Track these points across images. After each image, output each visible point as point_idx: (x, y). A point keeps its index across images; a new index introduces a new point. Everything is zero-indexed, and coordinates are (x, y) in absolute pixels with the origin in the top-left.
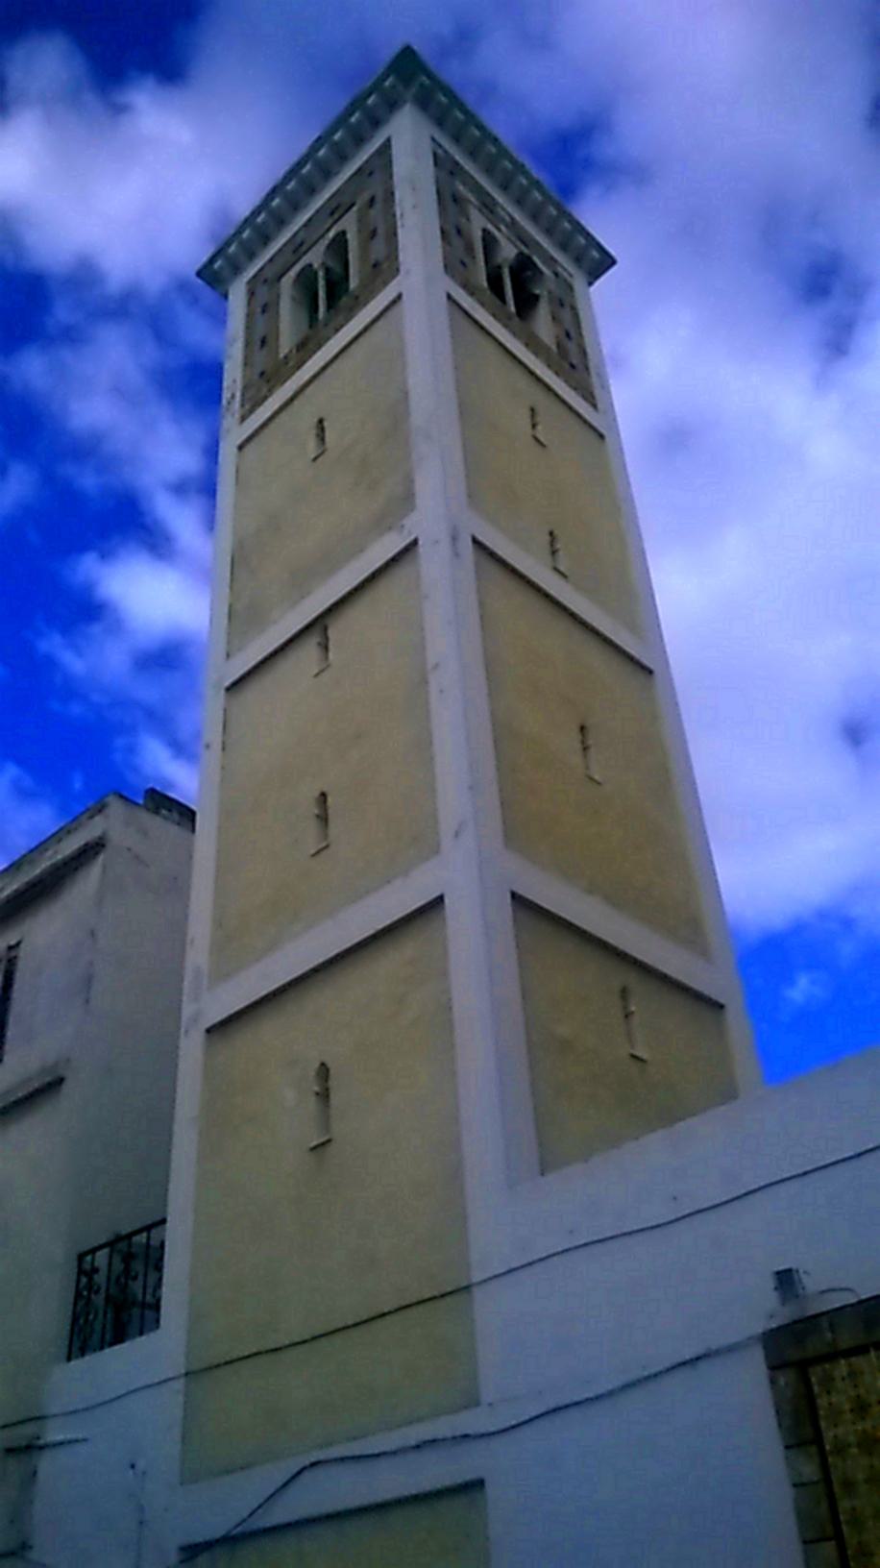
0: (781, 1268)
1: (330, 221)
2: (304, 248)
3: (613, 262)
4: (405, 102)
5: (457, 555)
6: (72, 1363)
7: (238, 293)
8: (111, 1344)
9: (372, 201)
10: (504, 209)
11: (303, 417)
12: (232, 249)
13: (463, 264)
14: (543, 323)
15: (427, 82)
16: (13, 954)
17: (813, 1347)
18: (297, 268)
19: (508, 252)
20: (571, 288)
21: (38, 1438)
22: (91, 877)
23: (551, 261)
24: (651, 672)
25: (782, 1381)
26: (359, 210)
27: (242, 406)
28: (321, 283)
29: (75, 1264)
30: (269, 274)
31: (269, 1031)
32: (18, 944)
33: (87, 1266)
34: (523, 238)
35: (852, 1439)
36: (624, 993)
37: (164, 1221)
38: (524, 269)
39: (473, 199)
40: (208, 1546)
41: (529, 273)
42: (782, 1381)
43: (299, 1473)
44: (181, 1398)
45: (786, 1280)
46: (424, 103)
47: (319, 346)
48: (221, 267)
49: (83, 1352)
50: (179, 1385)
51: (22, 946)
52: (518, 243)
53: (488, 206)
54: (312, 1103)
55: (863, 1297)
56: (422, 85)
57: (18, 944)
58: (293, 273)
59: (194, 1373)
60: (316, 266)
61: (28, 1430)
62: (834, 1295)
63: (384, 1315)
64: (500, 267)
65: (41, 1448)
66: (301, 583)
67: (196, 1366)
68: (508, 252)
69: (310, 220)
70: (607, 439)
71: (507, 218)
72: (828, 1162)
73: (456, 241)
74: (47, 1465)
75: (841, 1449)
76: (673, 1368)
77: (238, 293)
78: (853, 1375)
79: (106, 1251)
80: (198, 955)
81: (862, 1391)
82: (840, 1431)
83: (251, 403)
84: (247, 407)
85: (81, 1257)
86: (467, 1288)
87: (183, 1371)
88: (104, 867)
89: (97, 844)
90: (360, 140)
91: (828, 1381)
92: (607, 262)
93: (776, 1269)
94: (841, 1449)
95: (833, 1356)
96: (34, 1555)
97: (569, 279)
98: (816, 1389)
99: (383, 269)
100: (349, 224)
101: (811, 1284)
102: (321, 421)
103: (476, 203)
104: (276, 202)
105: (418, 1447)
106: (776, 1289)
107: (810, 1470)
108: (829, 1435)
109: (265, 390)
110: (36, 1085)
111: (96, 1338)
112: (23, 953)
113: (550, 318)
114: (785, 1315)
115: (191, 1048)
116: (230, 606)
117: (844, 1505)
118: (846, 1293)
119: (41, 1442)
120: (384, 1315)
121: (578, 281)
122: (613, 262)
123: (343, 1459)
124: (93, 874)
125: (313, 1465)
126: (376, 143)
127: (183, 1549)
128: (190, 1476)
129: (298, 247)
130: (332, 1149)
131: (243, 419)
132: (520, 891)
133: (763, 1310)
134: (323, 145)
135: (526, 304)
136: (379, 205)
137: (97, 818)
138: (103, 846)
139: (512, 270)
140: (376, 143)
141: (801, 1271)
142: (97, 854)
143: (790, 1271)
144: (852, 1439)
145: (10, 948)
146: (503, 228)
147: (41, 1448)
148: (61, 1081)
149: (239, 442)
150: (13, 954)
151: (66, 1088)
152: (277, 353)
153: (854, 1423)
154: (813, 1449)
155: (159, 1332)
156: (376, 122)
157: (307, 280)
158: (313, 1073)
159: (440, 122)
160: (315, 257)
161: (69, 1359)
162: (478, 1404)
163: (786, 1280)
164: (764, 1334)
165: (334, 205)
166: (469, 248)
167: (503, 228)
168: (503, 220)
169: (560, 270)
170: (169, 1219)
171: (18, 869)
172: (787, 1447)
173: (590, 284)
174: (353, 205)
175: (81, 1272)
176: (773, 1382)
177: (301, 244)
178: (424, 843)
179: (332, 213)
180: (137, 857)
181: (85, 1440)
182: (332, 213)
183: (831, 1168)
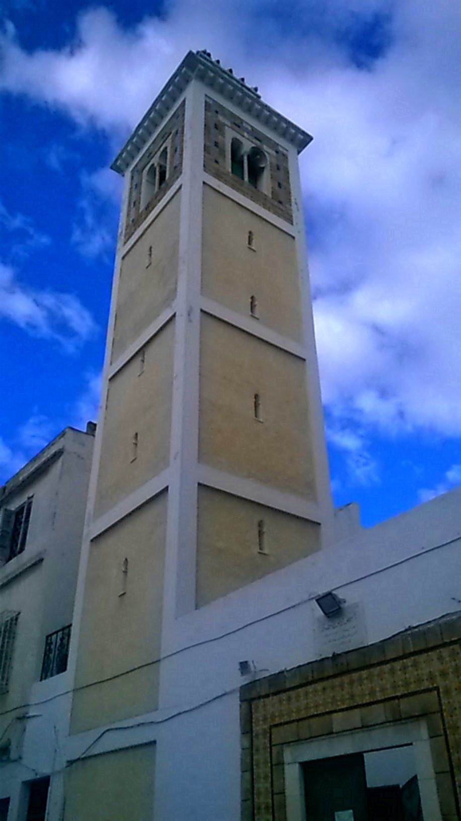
1: (162, 142)
2: (152, 155)
3: (311, 139)
4: (191, 80)
5: (190, 321)
6: (43, 681)
7: (128, 174)
8: (58, 673)
9: (177, 133)
10: (247, 123)
11: (143, 247)
12: (124, 155)
13: (216, 162)
14: (266, 183)
15: (202, 67)
16: (30, 500)
17: (254, 694)
18: (149, 166)
19: (247, 146)
20: (285, 157)
21: (27, 713)
22: (56, 469)
23: (275, 146)
24: (304, 360)
25: (243, 707)
26: (172, 136)
27: (125, 237)
28: (157, 173)
29: (45, 640)
30: (139, 167)
31: (111, 542)
32: (32, 496)
33: (49, 641)
34: (257, 136)
36: (260, 524)
37: (71, 625)
38: (256, 155)
39: (226, 123)
40: (75, 761)
41: (258, 157)
42: (243, 707)
43: (104, 733)
44: (71, 700)
46: (202, 77)
47: (153, 208)
48: (120, 164)
49: (45, 678)
50: (70, 695)
51: (34, 497)
52: (254, 141)
53: (238, 124)
54: (122, 575)
56: (199, 69)
57: (32, 496)
58: (147, 169)
59: (77, 689)
60: (156, 165)
61: (24, 710)
62: (263, 672)
63: (135, 669)
64: (243, 156)
65: (29, 717)
66: (137, 333)
67: (78, 687)
68: (247, 146)
69: (155, 140)
70: (296, 239)
71: (250, 128)
73: (214, 150)
74: (31, 725)
76: (215, 699)
77: (128, 174)
79: (61, 632)
80: (90, 507)
82: (258, 728)
83: (129, 236)
84: (127, 237)
85: (47, 637)
86: (159, 661)
87: (73, 688)
88: (63, 465)
89: (59, 452)
90: (174, 100)
92: (308, 139)
95: (259, 698)
96: (24, 761)
97: (285, 152)
99: (177, 170)
100: (168, 143)
102: (151, 248)
103: (229, 125)
104: (140, 132)
105: (138, 725)
106: (239, 669)
107: (247, 744)
109: (133, 229)
110: (33, 562)
111: (54, 672)
112: (34, 500)
113: (270, 176)
114: (245, 680)
115: (86, 546)
116: (114, 339)
118: (266, 672)
119: (27, 715)
120: (135, 669)
121: (291, 150)
122: (311, 139)
123: (117, 729)
124: (59, 465)
125: (108, 730)
126: (179, 102)
127: (68, 762)
128: (73, 730)
129: (150, 155)
130: (125, 596)
131: (125, 243)
132: (201, 482)
134: (157, 103)
135: (255, 174)
136: (179, 135)
137: (62, 439)
138: (62, 453)
139: (248, 156)
140: (179, 102)
142: (60, 456)
143: (246, 662)
145: (29, 498)
146: (246, 134)
147: (29, 717)
148: (41, 560)
149: (122, 256)
150: (30, 500)
151: (44, 563)
152: (139, 210)
154: (249, 735)
155: (66, 672)
156: (181, 90)
157: (152, 169)
158: (122, 563)
159: (211, 84)
160: (155, 160)
161: (41, 680)
162: (157, 710)
163: (244, 666)
164: (241, 687)
165: (163, 133)
166: (222, 153)
167: (246, 134)
168: (246, 130)
169: (281, 149)
170: (73, 625)
171: (35, 460)
172: (243, 733)
173: (299, 153)
174: (170, 133)
175: (47, 643)
177: (150, 154)
178: (161, 461)
179: (163, 138)
180: (79, 456)
181: (41, 715)
182: (163, 138)
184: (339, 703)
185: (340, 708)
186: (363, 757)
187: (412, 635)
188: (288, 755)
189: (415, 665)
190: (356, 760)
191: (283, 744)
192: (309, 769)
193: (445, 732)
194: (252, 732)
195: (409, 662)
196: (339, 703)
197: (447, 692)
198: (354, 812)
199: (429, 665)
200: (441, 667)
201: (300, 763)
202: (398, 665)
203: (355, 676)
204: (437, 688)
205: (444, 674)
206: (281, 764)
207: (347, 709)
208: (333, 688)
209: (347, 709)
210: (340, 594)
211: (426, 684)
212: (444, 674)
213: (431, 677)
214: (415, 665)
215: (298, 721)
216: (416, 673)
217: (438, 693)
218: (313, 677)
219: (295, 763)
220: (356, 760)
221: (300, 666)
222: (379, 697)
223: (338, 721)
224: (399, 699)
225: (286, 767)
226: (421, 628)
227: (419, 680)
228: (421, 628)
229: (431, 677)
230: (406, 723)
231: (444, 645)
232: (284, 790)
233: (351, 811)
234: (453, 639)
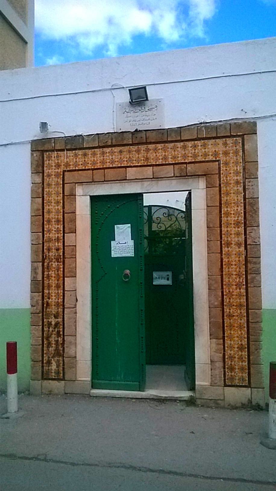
0: (44, 122)
17: (46, 147)
35: (53, 173)
45: (44, 125)
55: (66, 136)
72: (241, 74)
75: (49, 176)
78: (58, 157)
81: (59, 161)
91: (49, 158)
93: (42, 121)
94: (49, 176)
95: (47, 151)
98: (45, 159)
101: (50, 129)
107: (38, 180)
108: (46, 171)
117: (46, 190)
118: (63, 134)
133: (35, 133)
141: (48, 125)
144: (53, 173)
153: (55, 169)
163: (44, 125)
176: (32, 154)
183: (69, 95)
184: (134, 162)
185: (134, 165)
186: (143, 195)
187: (205, 127)
188: (79, 190)
189: (204, 146)
190: (139, 197)
191: (76, 183)
192: (93, 199)
193: (220, 185)
194: (43, 173)
195: (199, 143)
196: (134, 162)
197: (226, 164)
198: (152, 229)
199: (211, 147)
200: (224, 149)
201: (91, 196)
202: (190, 144)
203: (151, 146)
204: (218, 161)
205: (226, 153)
206: (73, 195)
207: (140, 166)
208: (130, 152)
209: (140, 166)
210: (150, 91)
211: (211, 158)
212: (226, 153)
213: (216, 154)
214: (204, 146)
215: (93, 170)
216: (203, 150)
217: (219, 164)
218: (112, 143)
219: (86, 195)
220: (139, 197)
221: (98, 134)
222: (170, 161)
223: (131, 173)
224: (93, 171)
225: (76, 197)
226: (212, 124)
227: (206, 155)
228: (212, 124)
229: (216, 154)
230: (188, 178)
231: (231, 136)
232: (75, 211)
233: (153, 230)
234: (239, 134)
